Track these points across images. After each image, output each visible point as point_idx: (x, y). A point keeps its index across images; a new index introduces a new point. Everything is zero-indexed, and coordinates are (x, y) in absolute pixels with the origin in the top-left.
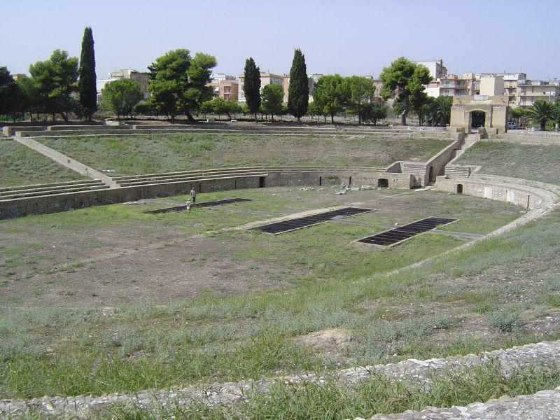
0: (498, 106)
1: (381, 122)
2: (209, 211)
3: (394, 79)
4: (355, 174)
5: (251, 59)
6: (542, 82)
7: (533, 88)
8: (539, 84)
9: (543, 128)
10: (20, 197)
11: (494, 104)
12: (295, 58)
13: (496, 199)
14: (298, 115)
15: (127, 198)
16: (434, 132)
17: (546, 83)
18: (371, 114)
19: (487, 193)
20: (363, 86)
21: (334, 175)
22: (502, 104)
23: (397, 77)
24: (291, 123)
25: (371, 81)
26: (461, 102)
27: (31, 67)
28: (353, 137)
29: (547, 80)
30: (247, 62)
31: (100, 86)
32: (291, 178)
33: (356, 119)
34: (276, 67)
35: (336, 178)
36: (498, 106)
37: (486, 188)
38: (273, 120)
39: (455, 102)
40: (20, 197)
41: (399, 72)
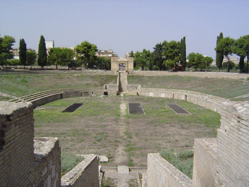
0: (130, 61)
1: (78, 68)
2: (69, 104)
3: (84, 50)
4: (95, 90)
5: (23, 39)
6: (105, 51)
7: (103, 53)
8: (104, 52)
9: (143, 69)
10: (45, 96)
11: (128, 60)
12: (41, 39)
13: (155, 96)
14: (42, 66)
15: (39, 101)
16: (108, 73)
17: (107, 51)
18: (73, 65)
19: (151, 95)
20: (70, 53)
21: (87, 91)
22: (131, 60)
23: (85, 49)
24: (38, 69)
25: (70, 51)
26: (114, 60)
27: (215, 49)
28: (76, 75)
29: (106, 50)
30: (21, 41)
31: (187, 55)
32: (71, 93)
33: (67, 68)
34: (33, 46)
35: (87, 92)
36: (130, 61)
37: (150, 93)
38: (31, 69)
39: (112, 60)
40: (45, 96)
41: (86, 47)
